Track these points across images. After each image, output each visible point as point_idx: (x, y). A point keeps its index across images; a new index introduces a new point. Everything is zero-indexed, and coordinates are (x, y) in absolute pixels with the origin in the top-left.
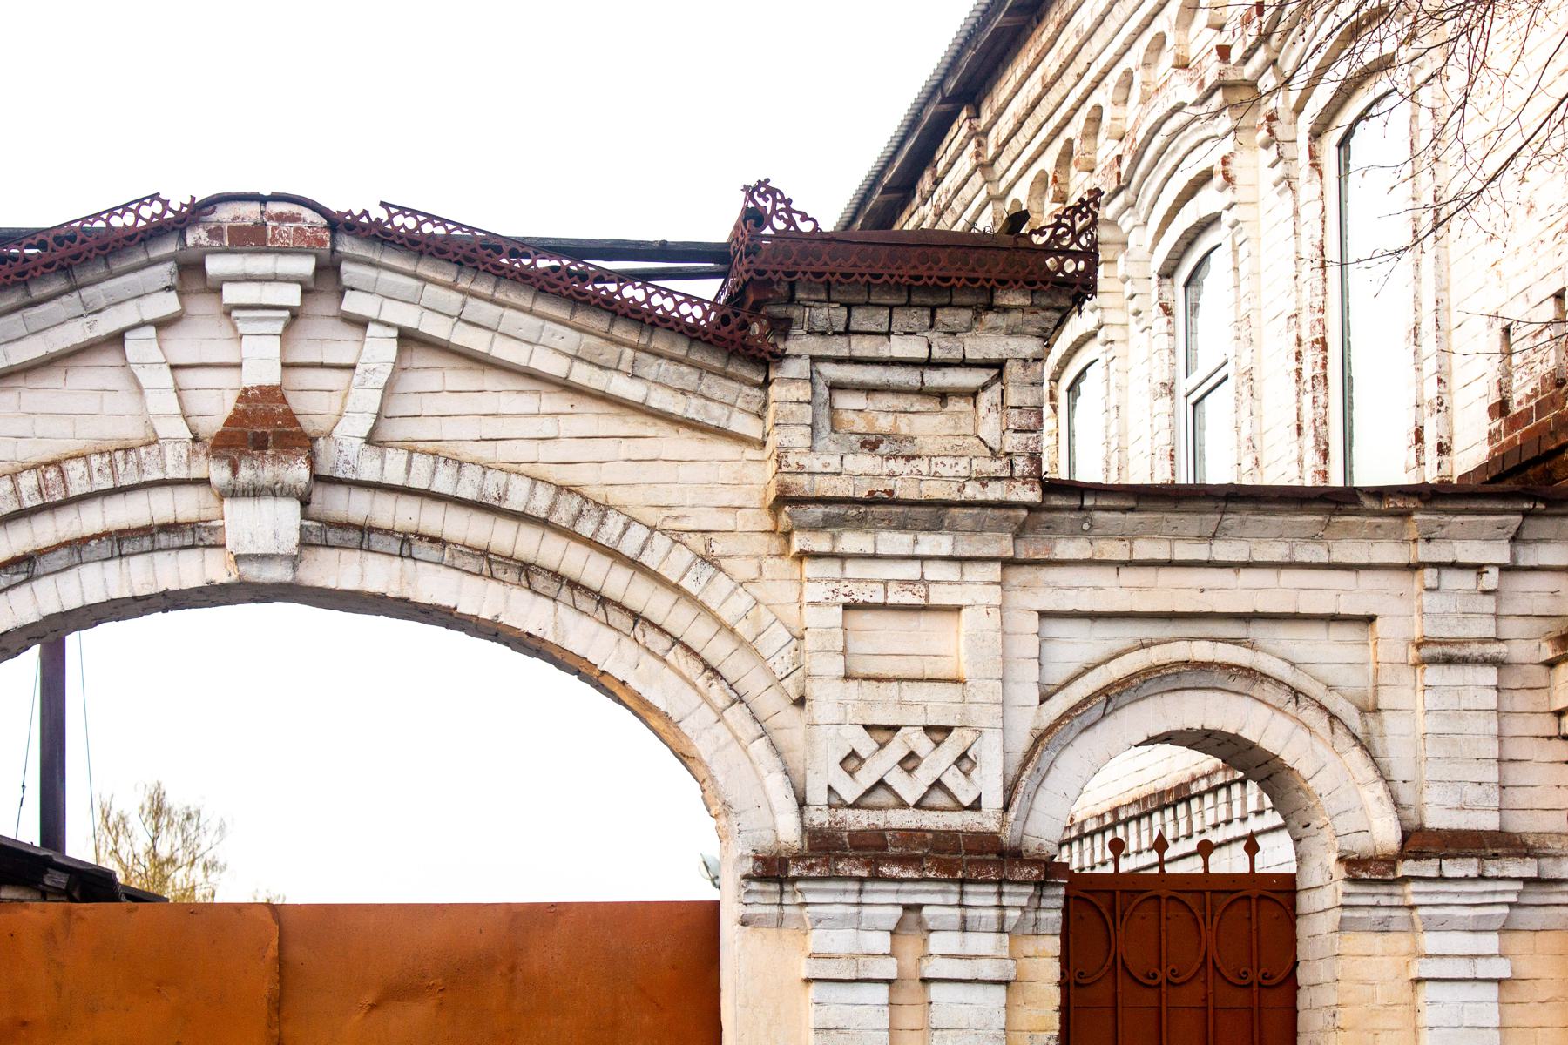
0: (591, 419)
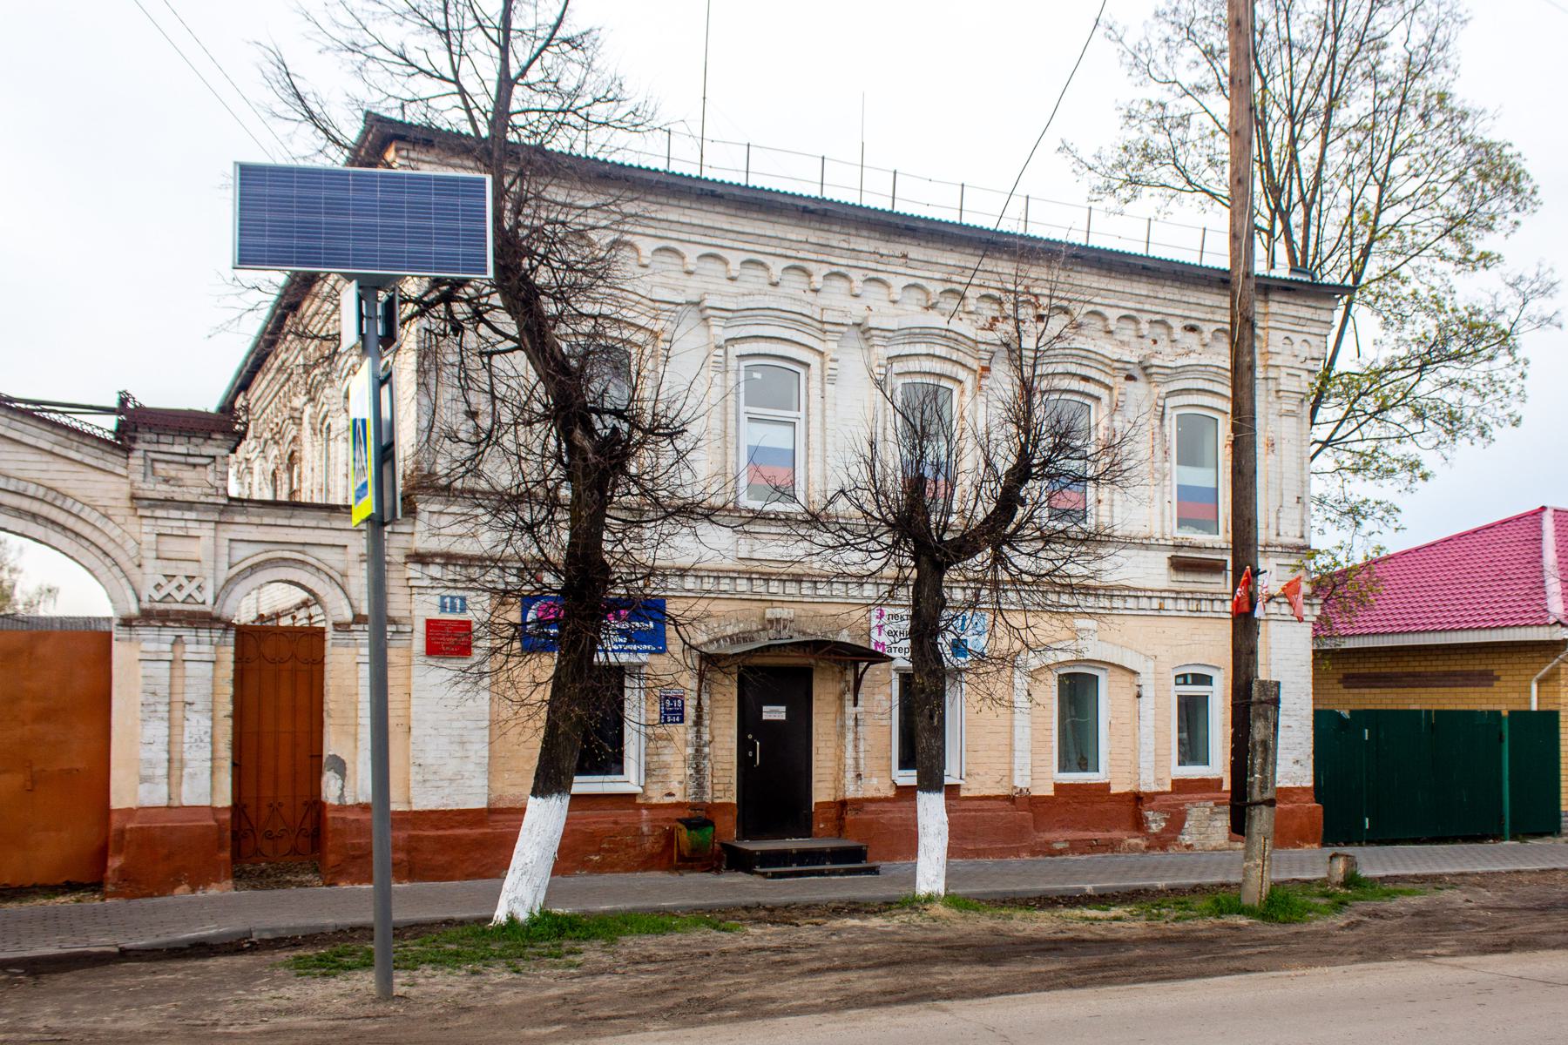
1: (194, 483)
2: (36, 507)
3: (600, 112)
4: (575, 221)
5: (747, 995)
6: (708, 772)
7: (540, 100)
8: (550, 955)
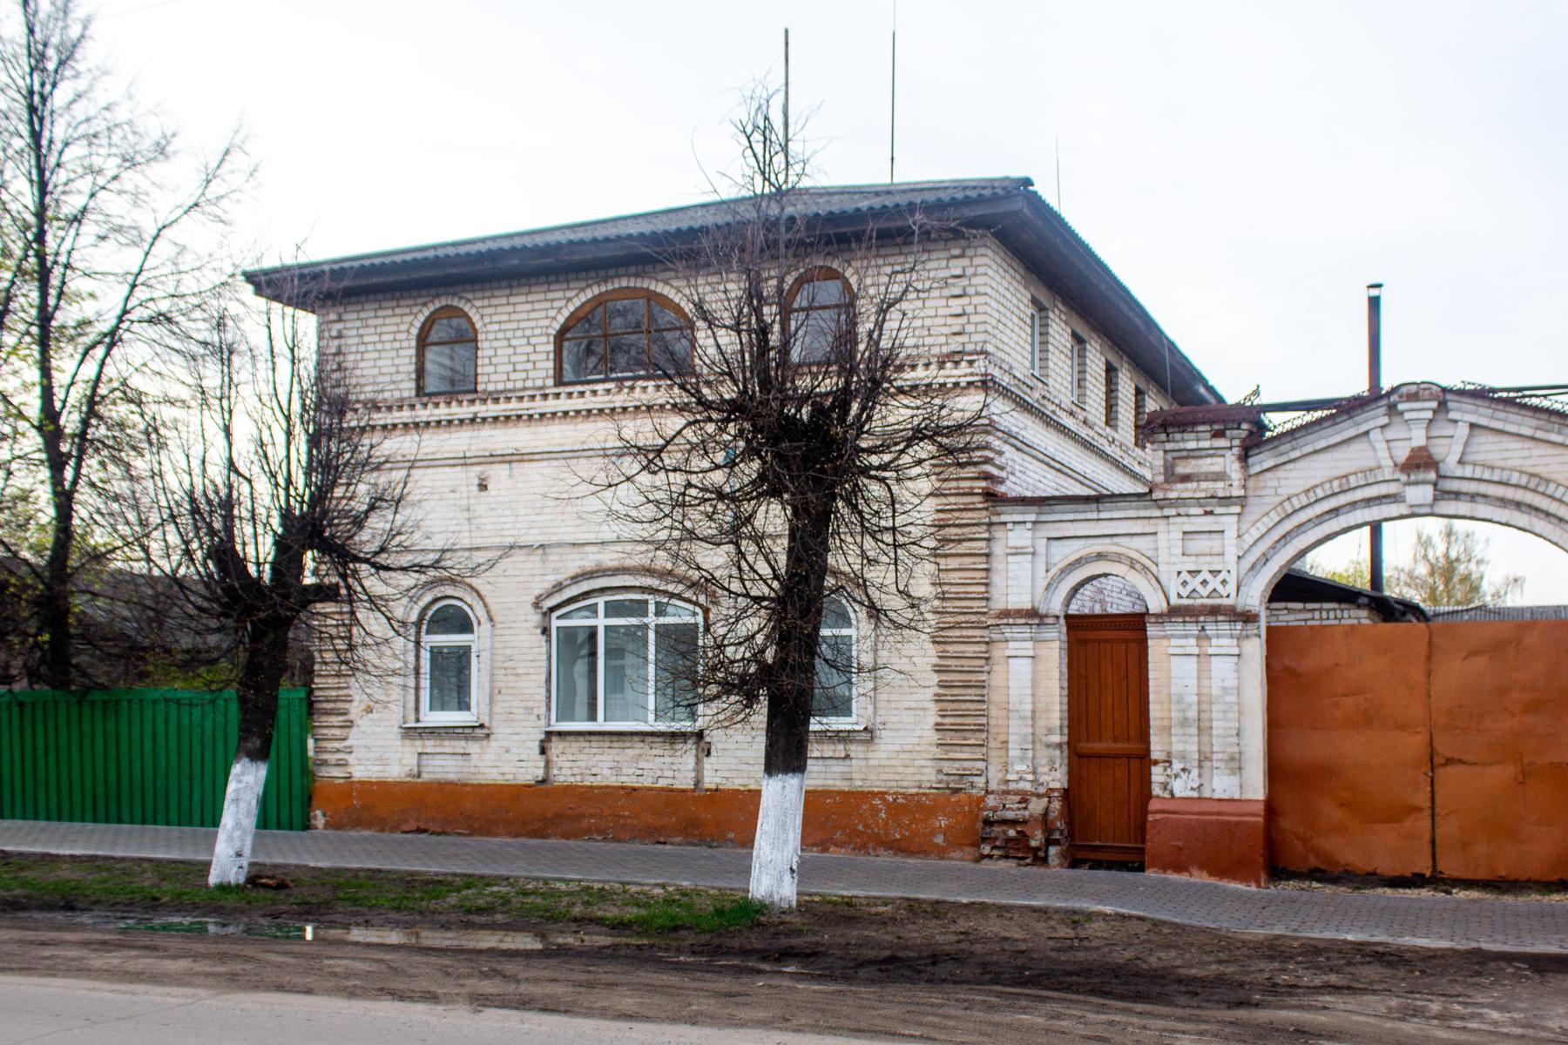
0: (1542, 450)
2: (1519, 495)
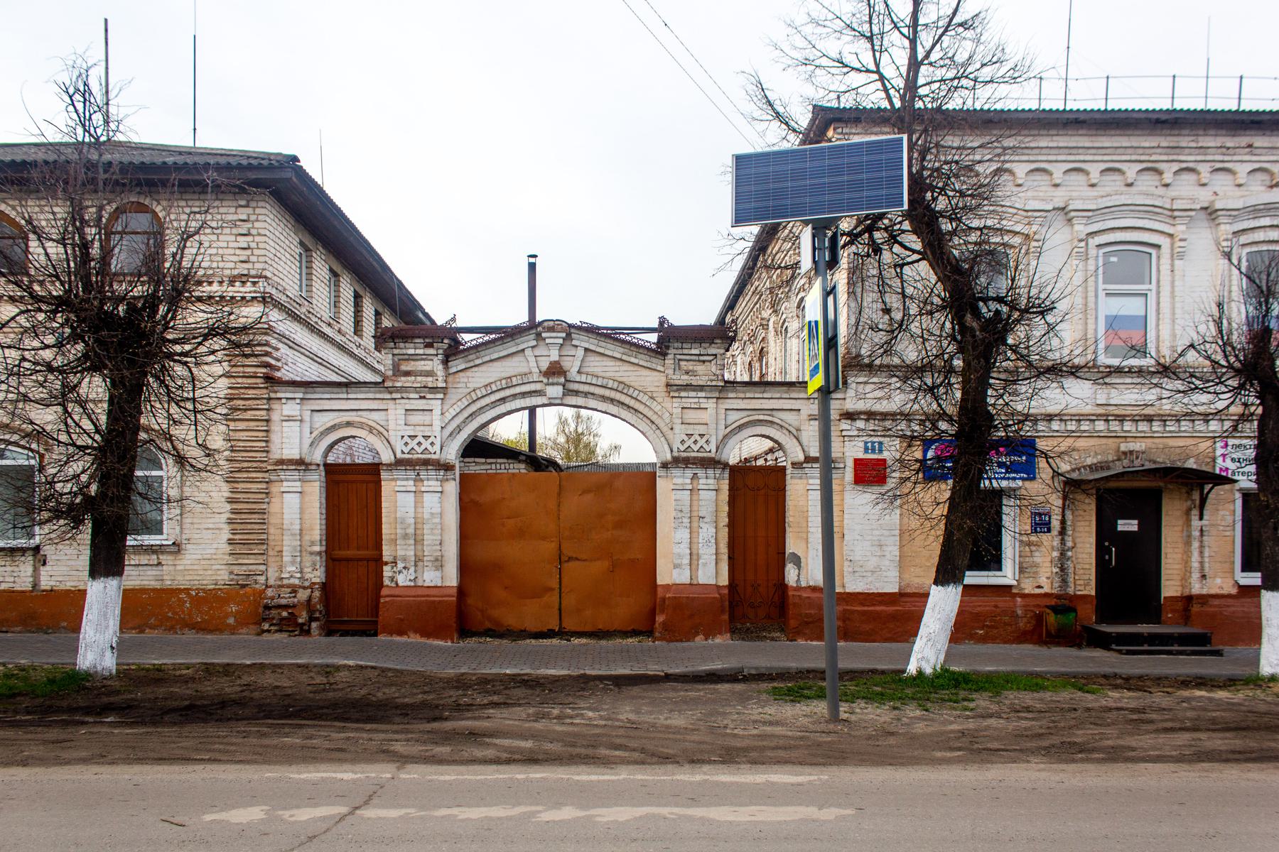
1: (704, 373)
2: (613, 394)
3: (986, 73)
4: (967, 159)
5: (1110, 743)
6: (1071, 570)
7: (940, 73)
8: (950, 700)
